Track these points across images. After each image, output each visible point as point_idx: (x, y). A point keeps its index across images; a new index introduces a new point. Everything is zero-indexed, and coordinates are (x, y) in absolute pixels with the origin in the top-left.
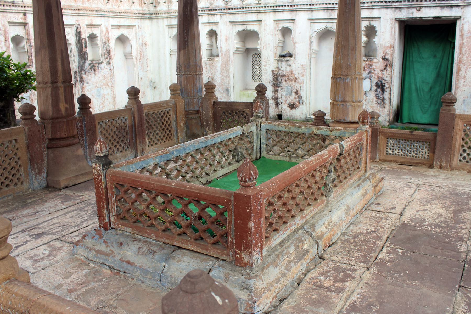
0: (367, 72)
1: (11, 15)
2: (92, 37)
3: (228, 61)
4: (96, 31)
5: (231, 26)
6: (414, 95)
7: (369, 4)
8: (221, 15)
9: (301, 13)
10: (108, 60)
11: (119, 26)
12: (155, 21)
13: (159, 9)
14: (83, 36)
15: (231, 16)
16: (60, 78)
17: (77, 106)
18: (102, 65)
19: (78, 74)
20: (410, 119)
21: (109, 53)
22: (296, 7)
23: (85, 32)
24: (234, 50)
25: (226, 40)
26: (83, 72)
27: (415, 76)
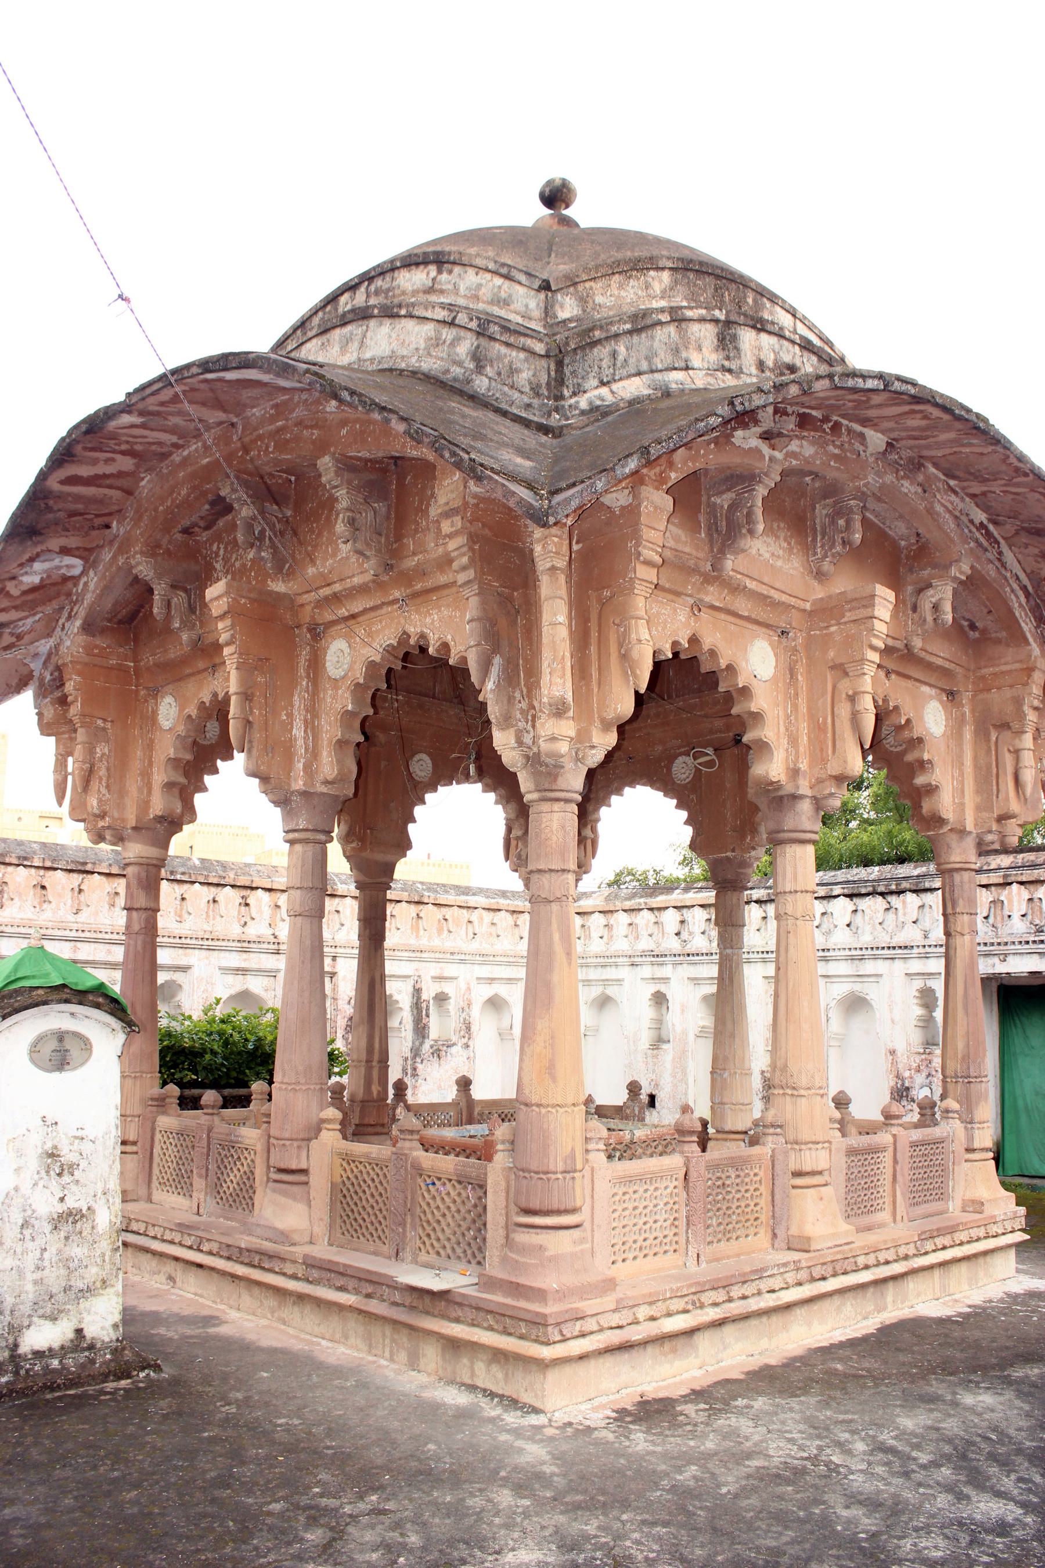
0: (924, 1074)
2: (441, 998)
3: (684, 1052)
4: (448, 988)
5: (691, 987)
6: (1023, 1119)
7: (921, 950)
8: (675, 964)
10: (465, 1040)
11: (491, 980)
14: (424, 996)
15: (691, 968)
16: (376, 1057)
17: (391, 1092)
18: (454, 1050)
19: (409, 1062)
20: (1021, 1168)
21: (468, 1028)
24: (697, 1031)
25: (683, 1011)
26: (418, 1060)
27: (1021, 1081)
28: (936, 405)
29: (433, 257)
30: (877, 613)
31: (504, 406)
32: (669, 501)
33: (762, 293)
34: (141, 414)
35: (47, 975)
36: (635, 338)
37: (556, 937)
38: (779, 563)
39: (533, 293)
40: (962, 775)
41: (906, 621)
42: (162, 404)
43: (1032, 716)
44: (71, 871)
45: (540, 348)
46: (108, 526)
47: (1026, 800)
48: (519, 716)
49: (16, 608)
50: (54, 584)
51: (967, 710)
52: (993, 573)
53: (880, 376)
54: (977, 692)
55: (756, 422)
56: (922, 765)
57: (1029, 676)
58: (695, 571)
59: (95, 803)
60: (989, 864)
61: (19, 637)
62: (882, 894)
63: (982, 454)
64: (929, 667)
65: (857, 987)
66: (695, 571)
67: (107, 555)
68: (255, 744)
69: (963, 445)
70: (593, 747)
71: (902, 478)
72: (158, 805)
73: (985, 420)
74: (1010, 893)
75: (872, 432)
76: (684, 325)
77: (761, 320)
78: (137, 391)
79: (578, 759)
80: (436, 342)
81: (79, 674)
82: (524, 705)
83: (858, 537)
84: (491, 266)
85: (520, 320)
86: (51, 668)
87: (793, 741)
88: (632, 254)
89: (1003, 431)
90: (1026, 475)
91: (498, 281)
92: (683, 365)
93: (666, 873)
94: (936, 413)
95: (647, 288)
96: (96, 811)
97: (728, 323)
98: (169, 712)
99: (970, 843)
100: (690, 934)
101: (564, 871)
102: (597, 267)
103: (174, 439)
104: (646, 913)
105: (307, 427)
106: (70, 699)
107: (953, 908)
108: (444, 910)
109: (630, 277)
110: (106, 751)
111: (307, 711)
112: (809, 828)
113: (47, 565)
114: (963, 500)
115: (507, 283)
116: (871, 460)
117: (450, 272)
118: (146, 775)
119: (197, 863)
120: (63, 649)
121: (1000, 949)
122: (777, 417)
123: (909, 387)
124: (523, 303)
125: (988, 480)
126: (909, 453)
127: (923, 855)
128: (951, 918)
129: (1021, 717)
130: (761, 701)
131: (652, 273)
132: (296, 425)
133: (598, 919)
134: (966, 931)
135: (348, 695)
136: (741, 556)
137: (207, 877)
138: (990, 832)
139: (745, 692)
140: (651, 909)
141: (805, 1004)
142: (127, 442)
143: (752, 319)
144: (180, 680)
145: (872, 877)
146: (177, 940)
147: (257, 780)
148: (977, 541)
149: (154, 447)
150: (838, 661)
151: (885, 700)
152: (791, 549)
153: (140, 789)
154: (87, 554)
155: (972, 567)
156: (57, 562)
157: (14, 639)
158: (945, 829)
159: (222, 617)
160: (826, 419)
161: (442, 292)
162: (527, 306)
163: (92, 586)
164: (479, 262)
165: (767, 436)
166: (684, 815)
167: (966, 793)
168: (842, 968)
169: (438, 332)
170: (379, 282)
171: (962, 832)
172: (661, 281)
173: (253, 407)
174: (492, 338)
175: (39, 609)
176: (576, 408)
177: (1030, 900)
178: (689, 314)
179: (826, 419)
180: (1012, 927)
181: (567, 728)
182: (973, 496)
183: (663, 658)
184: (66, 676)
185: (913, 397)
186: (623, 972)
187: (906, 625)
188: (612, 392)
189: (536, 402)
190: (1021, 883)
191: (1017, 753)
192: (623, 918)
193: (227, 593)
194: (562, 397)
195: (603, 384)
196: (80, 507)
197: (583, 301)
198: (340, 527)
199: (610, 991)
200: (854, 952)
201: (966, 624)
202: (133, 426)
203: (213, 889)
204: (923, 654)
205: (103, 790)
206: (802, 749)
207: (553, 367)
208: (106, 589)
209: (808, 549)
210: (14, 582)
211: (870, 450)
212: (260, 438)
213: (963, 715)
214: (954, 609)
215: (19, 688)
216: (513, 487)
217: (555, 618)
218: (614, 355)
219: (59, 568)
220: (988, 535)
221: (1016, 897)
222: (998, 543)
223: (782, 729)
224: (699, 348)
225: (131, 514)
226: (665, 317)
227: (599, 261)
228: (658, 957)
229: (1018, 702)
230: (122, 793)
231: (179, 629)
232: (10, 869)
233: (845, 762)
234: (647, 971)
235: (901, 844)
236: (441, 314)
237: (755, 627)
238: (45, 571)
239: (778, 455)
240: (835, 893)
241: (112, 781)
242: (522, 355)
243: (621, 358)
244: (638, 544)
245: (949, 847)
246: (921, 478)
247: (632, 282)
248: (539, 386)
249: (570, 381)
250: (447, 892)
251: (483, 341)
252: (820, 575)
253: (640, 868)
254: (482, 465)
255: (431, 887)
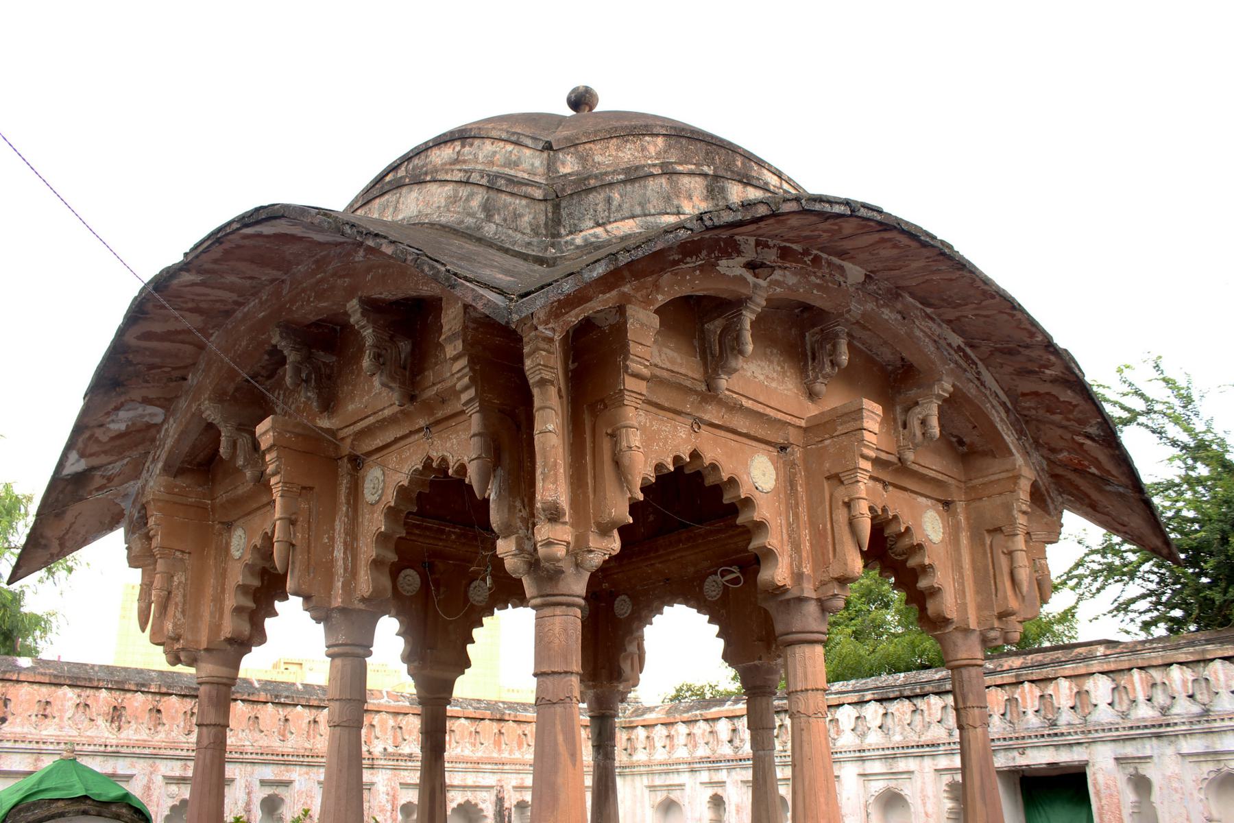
1: (406, 773)
7: (947, 747)
8: (729, 769)
9: (848, 764)
12: (629, 778)
13: (635, 758)
14: (507, 805)
22: (839, 755)
23: (510, 798)
25: (738, 811)
28: (903, 232)
29: (462, 136)
30: (865, 425)
31: (507, 246)
32: (656, 321)
33: (749, 157)
34: (199, 272)
35: (71, 786)
36: (629, 187)
37: (560, 738)
38: (774, 385)
39: (538, 153)
40: (962, 577)
41: (898, 437)
42: (215, 261)
43: (1021, 520)
44: (184, 696)
45: (538, 194)
46: (184, 379)
47: (1023, 597)
48: (519, 524)
49: (105, 452)
50: (139, 431)
51: (962, 518)
52: (973, 391)
53: (847, 203)
54: (969, 502)
55: (739, 253)
56: (925, 570)
57: (1016, 484)
58: (690, 391)
59: (170, 627)
60: (1002, 666)
61: (110, 479)
62: (908, 698)
63: (951, 280)
64: (923, 478)
65: (892, 784)
66: (690, 391)
67: (183, 404)
68: (297, 565)
69: (934, 272)
70: (591, 552)
71: (882, 306)
72: (228, 627)
73: (950, 247)
74: (1023, 691)
75: (850, 265)
76: (675, 177)
77: (747, 176)
78: (192, 250)
79: (578, 565)
80: (454, 199)
81: (159, 510)
82: (524, 514)
83: (844, 358)
84: (504, 136)
85: (526, 176)
86: (139, 506)
87: (796, 546)
88: (634, 127)
89: (967, 257)
90: (993, 297)
91: (510, 147)
92: (675, 210)
93: (721, 688)
94: (904, 240)
95: (643, 150)
96: (171, 634)
97: (716, 177)
98: (240, 544)
99: (975, 640)
100: (742, 740)
101: (566, 672)
102: (595, 133)
103: (234, 297)
104: (702, 724)
105: (340, 277)
106: (152, 533)
107: (964, 702)
108: (524, 726)
109: (627, 141)
110: (183, 579)
111: (346, 534)
112: (815, 628)
113: (131, 414)
114: (940, 326)
115: (517, 148)
116: (852, 289)
117: (471, 145)
118: (219, 600)
119: (300, 687)
120: (148, 489)
121: (1018, 743)
122: (759, 249)
123: (875, 214)
124: (531, 162)
125: (960, 305)
126: (887, 284)
127: (940, 661)
128: (962, 712)
129: (1012, 522)
130: (764, 511)
131: (647, 138)
132: (332, 276)
133: (660, 731)
134: (978, 724)
135: (382, 518)
136: (735, 376)
137: (308, 700)
138: (993, 629)
139: (748, 502)
140: (706, 720)
141: (822, 800)
142: (193, 300)
143: (739, 174)
144: (249, 514)
145: (899, 682)
146: (280, 758)
147: (301, 599)
148: (956, 363)
149: (218, 305)
150: (833, 472)
151: (884, 510)
152: (784, 373)
153: (212, 614)
154: (167, 403)
155: (953, 386)
156: (140, 411)
157: (105, 481)
158: (951, 628)
159: (269, 449)
160: (806, 252)
161: (464, 162)
162: (532, 165)
163: (171, 432)
164: (494, 134)
165: (752, 266)
166: (716, 628)
167: (968, 594)
168: (877, 767)
169: (456, 191)
170: (416, 161)
171: (966, 631)
172: (655, 145)
173: (298, 264)
174: (499, 191)
175: (127, 453)
176: (572, 244)
177: (1042, 696)
178: (680, 168)
179: (806, 252)
180: (1027, 722)
181: (564, 533)
182: (949, 322)
183: (665, 471)
184: (149, 513)
185: (880, 223)
186: (685, 778)
187: (898, 441)
188: (607, 231)
189: (535, 240)
190: (1032, 681)
191: (1010, 554)
192: (682, 729)
193: (273, 428)
194: (559, 235)
195: (598, 225)
196: (157, 360)
197: (583, 159)
198: (366, 362)
199: (674, 795)
200: (887, 752)
201: (954, 440)
202: (193, 284)
203: (314, 711)
204: (916, 467)
205: (179, 615)
206: (804, 554)
207: (550, 209)
208: (183, 434)
209: (802, 371)
210: (103, 429)
211: (850, 281)
212: (304, 290)
213: (958, 522)
214: (942, 426)
215: (111, 527)
216: (481, 291)
217: (550, 427)
218: (609, 201)
219: (142, 416)
220: (966, 356)
221: (1029, 695)
222: (976, 364)
223: (785, 537)
224: (690, 198)
225: (202, 366)
226: (656, 171)
227: (599, 127)
228: (713, 763)
229: (1008, 508)
230: (197, 617)
231: (244, 466)
232: (129, 695)
233: (846, 564)
234: (704, 776)
235: (923, 652)
236: (458, 176)
237: (754, 444)
238: (131, 419)
239: (761, 282)
240: (867, 698)
241: (187, 606)
242: (524, 202)
243: (615, 203)
244: (626, 359)
245: (955, 645)
246: (899, 306)
247: (628, 146)
248: (538, 226)
249: (567, 222)
250: (525, 710)
251: (492, 194)
252: (812, 395)
253: (697, 684)
254: (455, 274)
255: (511, 706)
